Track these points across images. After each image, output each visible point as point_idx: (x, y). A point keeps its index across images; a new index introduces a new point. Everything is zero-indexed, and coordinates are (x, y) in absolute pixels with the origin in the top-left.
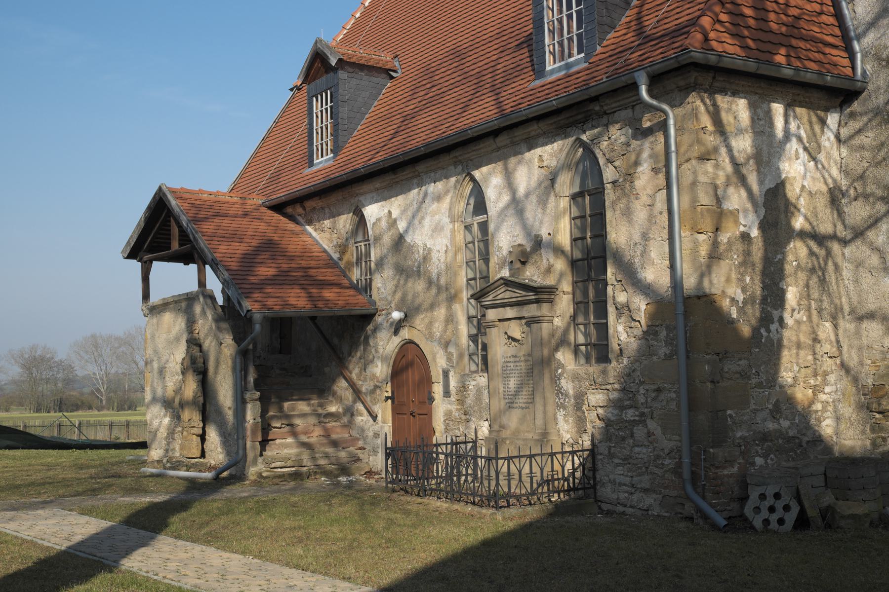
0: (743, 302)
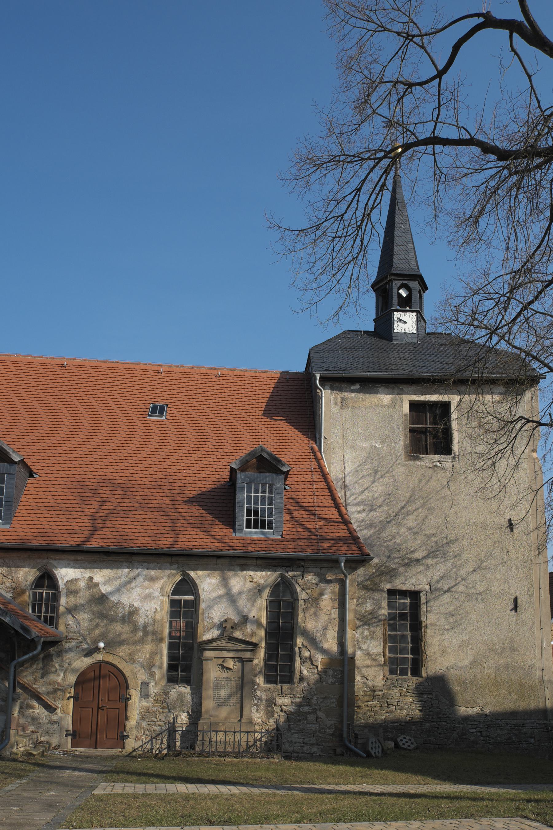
0: (23, 601)
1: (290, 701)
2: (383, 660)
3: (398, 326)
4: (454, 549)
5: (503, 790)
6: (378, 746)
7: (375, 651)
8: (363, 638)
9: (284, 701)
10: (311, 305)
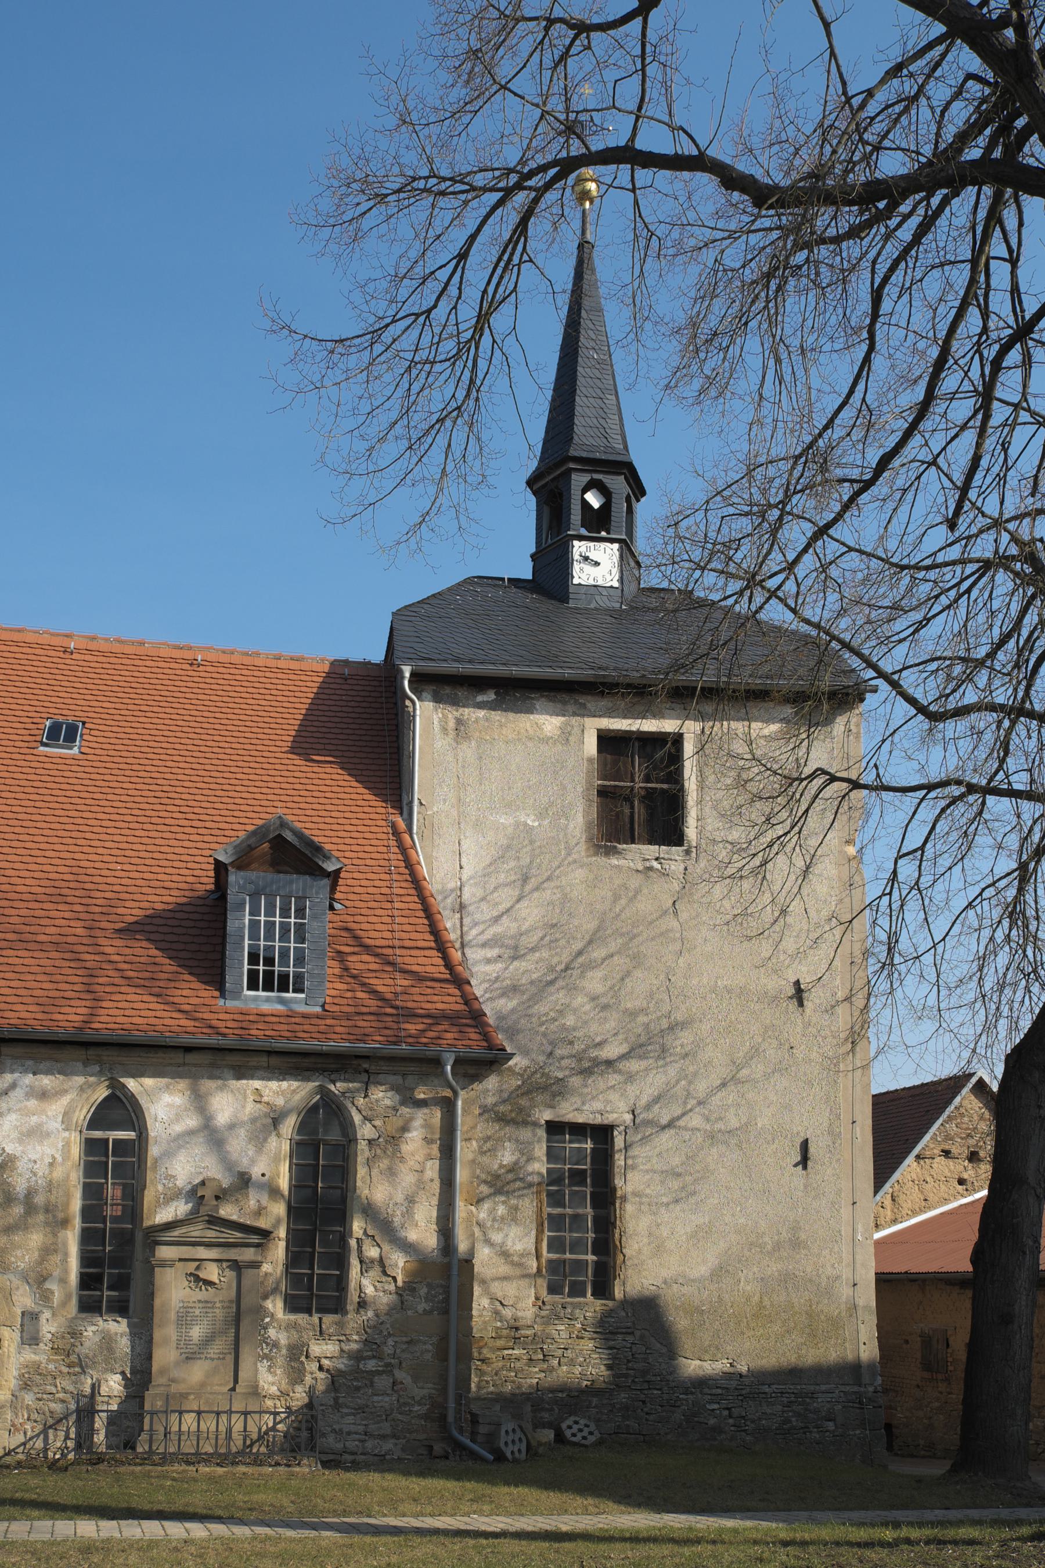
1: (337, 1348)
2: (535, 1265)
3: (581, 570)
4: (685, 1038)
5: (749, 1523)
6: (520, 1440)
7: (519, 1247)
8: (494, 1220)
9: (324, 1349)
10: (362, 508)
